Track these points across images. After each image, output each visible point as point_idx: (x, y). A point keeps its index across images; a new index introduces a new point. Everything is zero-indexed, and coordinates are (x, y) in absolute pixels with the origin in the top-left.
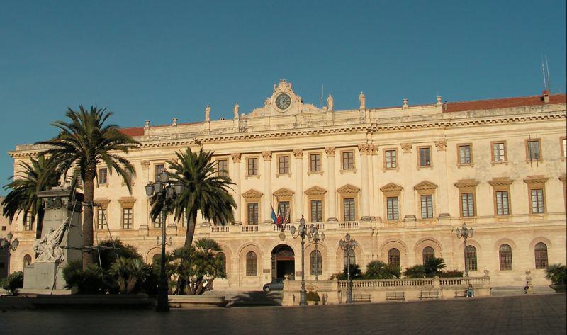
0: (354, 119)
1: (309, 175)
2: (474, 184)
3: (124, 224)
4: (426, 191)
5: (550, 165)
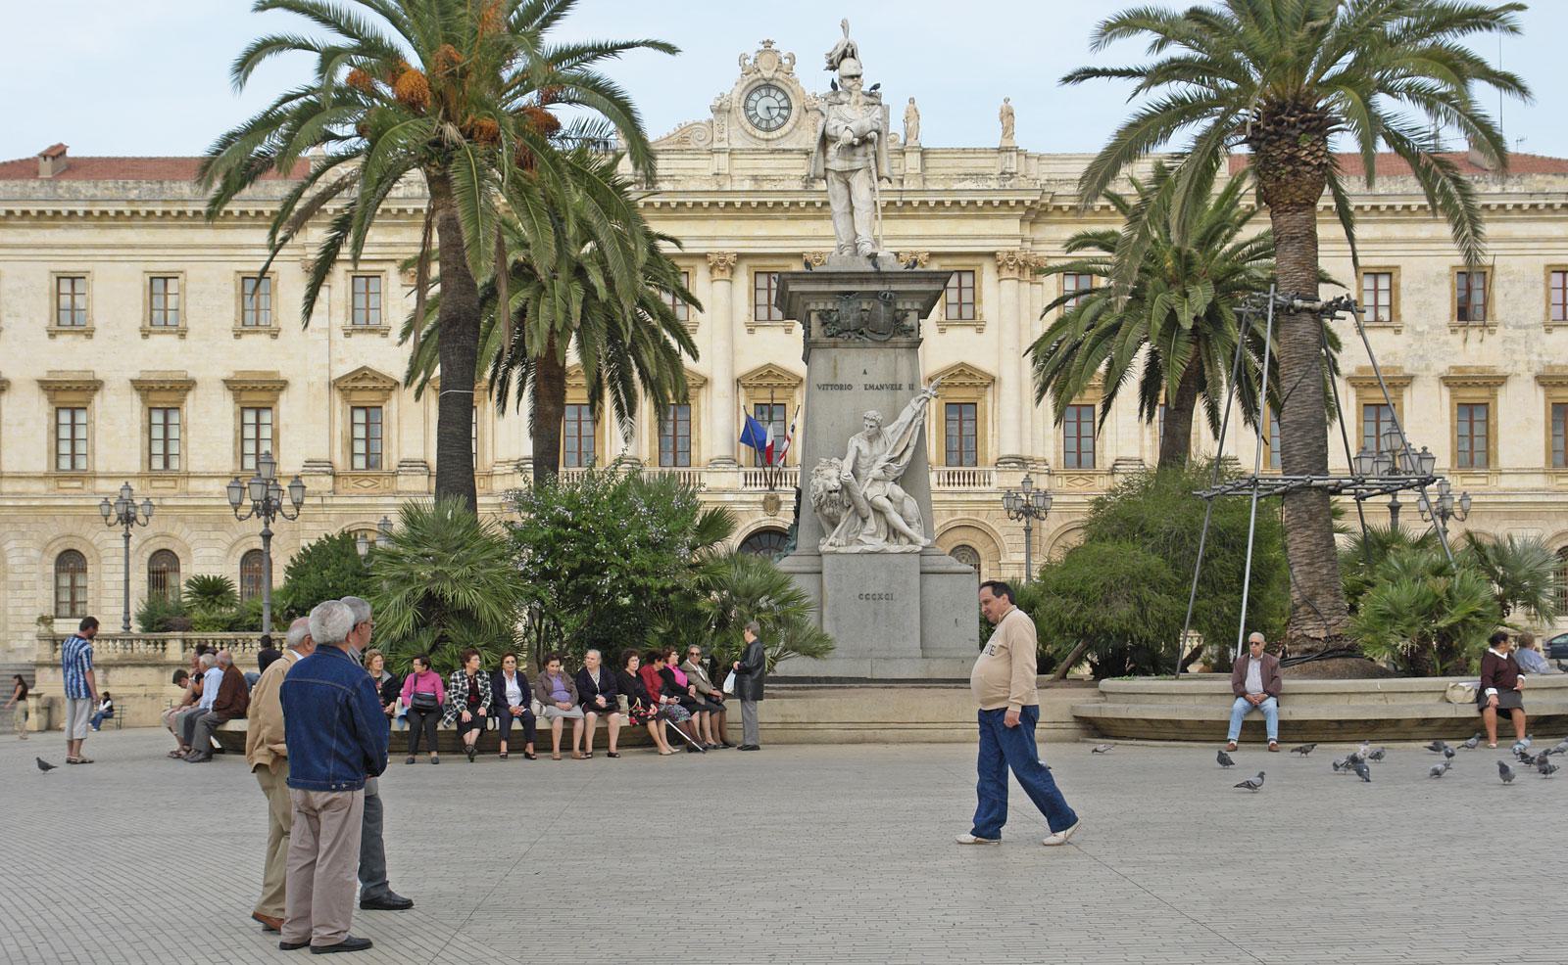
0: (984, 176)
1: (751, 331)
2: (1495, 382)
3: (58, 455)
4: (255, 395)
5: (1513, 341)
